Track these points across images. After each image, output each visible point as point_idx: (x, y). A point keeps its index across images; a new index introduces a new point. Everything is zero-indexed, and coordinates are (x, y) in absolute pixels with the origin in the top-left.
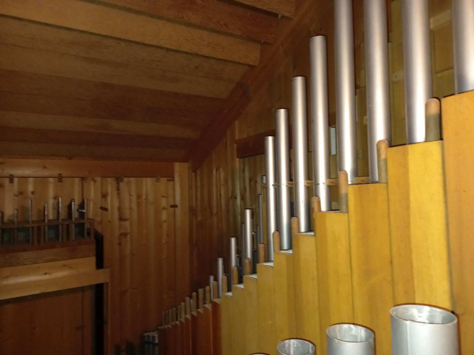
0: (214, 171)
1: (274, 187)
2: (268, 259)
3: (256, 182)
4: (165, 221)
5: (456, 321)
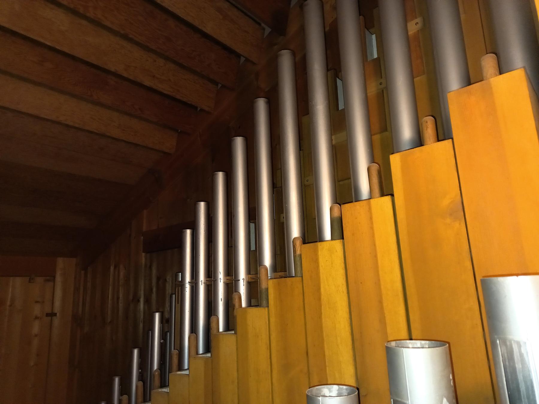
0: (112, 268)
1: (190, 285)
2: (180, 367)
3: (166, 280)
4: (36, 336)
5: (357, 393)
